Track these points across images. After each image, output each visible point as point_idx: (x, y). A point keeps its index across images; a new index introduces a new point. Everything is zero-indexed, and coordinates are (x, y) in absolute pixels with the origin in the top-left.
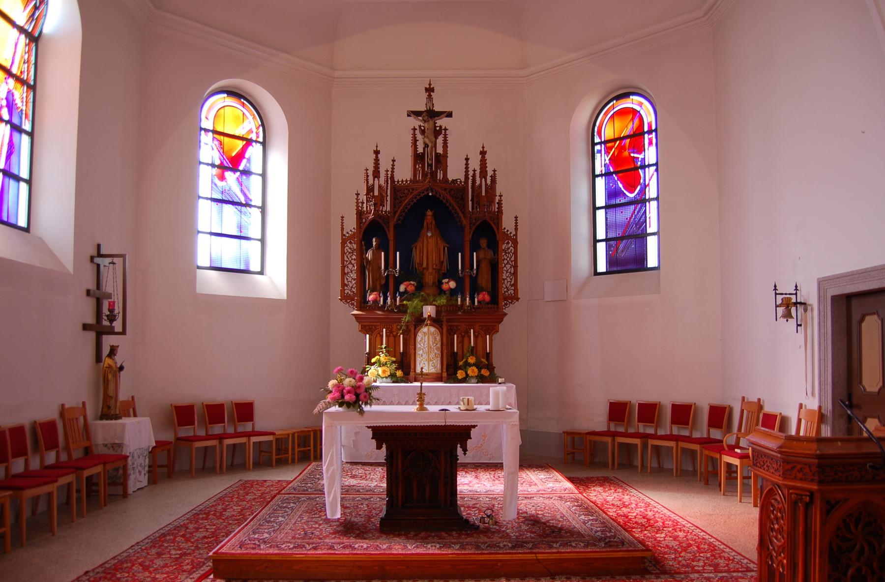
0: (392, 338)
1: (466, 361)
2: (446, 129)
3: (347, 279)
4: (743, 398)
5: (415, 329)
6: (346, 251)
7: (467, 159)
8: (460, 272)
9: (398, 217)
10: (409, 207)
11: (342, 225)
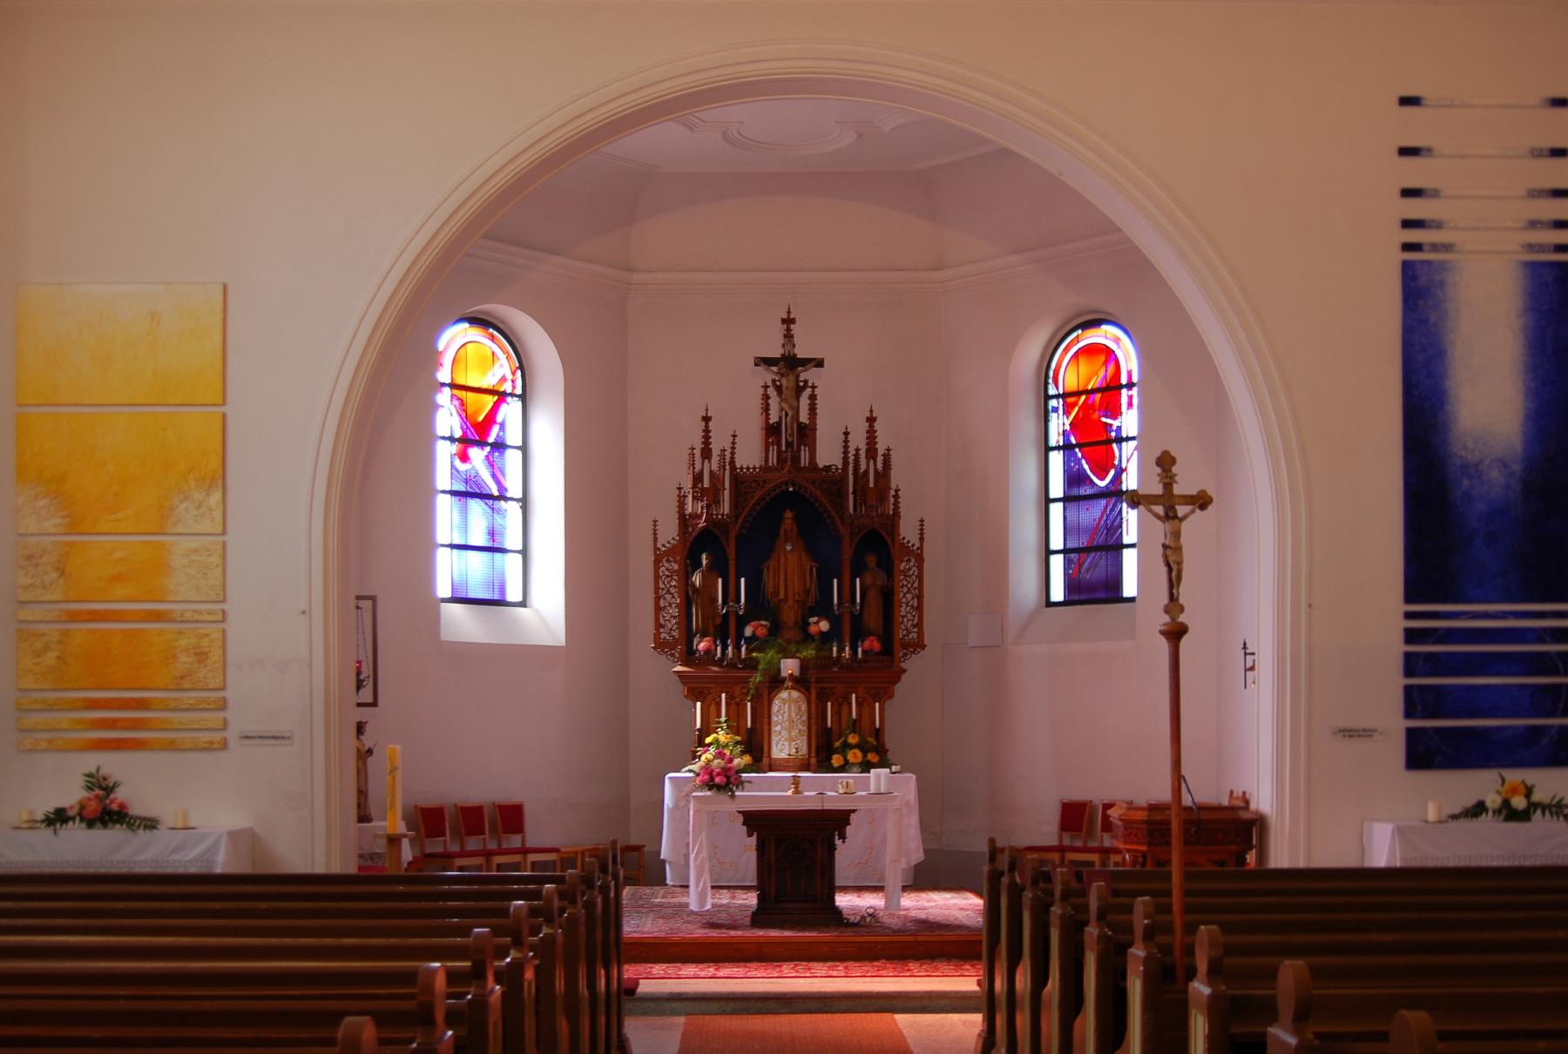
0: (733, 707)
1: (845, 741)
2: (814, 387)
4: (1232, 792)
5: (769, 694)
6: (661, 574)
7: (846, 434)
8: (836, 608)
9: (743, 523)
10: (758, 508)
11: (655, 534)
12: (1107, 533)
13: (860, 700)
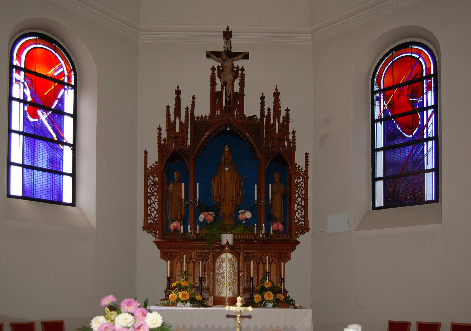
3: (150, 210)
6: (149, 184)
12: (413, 164)
13: (271, 261)
